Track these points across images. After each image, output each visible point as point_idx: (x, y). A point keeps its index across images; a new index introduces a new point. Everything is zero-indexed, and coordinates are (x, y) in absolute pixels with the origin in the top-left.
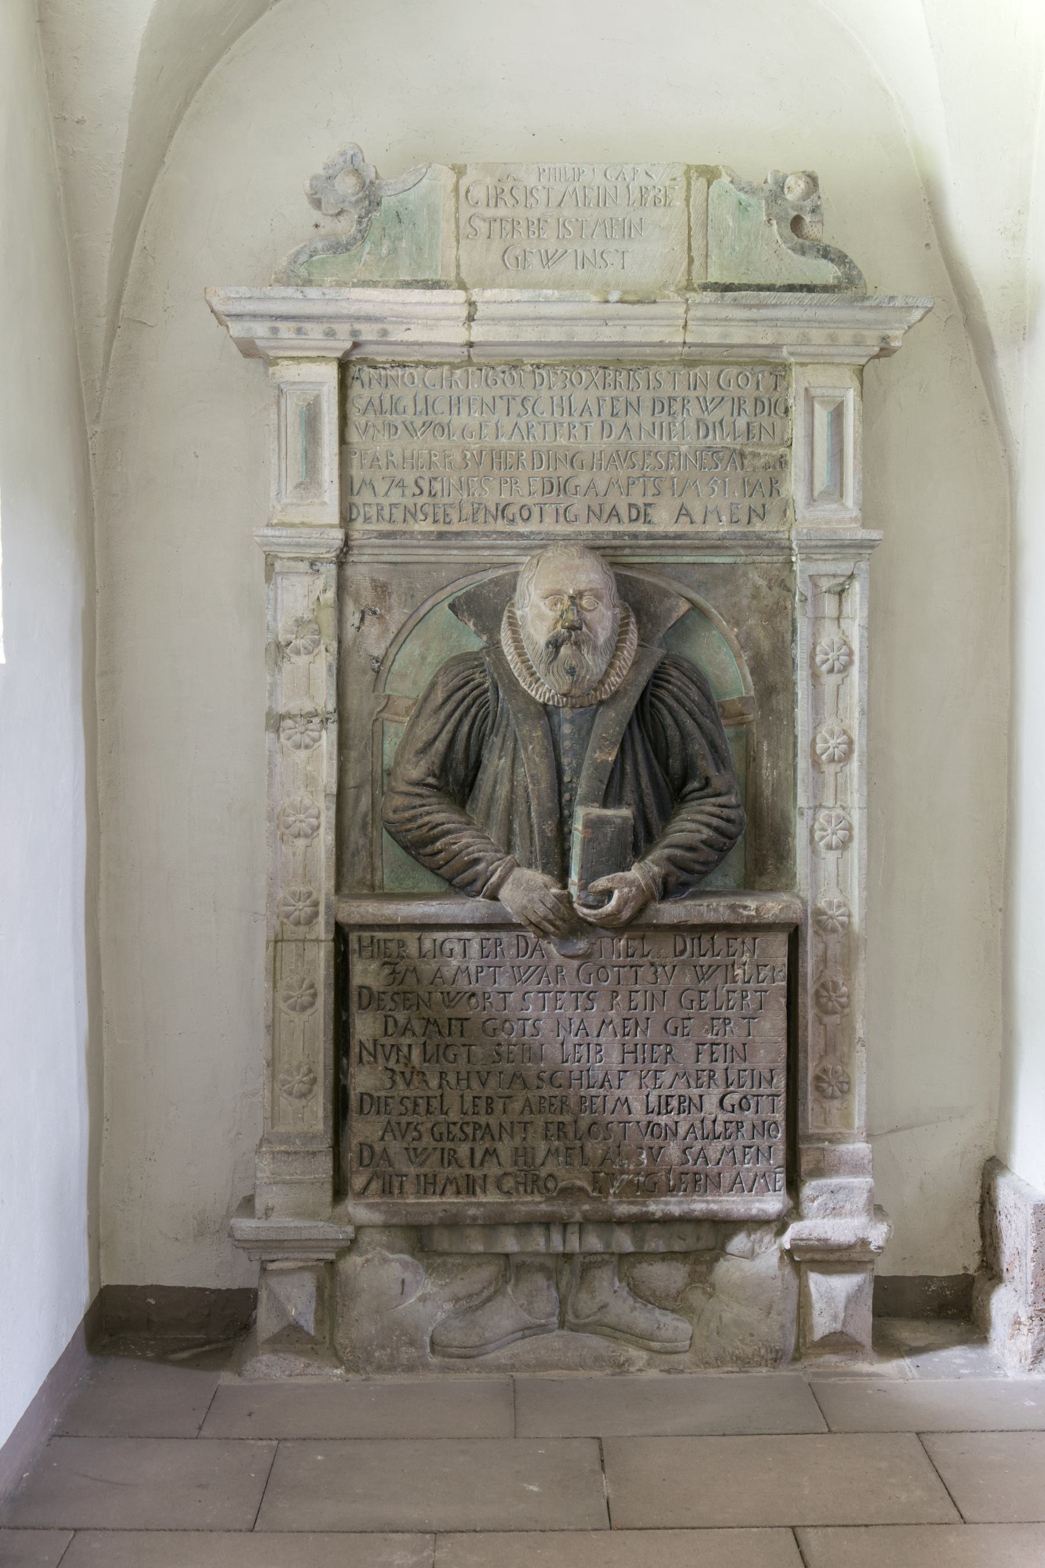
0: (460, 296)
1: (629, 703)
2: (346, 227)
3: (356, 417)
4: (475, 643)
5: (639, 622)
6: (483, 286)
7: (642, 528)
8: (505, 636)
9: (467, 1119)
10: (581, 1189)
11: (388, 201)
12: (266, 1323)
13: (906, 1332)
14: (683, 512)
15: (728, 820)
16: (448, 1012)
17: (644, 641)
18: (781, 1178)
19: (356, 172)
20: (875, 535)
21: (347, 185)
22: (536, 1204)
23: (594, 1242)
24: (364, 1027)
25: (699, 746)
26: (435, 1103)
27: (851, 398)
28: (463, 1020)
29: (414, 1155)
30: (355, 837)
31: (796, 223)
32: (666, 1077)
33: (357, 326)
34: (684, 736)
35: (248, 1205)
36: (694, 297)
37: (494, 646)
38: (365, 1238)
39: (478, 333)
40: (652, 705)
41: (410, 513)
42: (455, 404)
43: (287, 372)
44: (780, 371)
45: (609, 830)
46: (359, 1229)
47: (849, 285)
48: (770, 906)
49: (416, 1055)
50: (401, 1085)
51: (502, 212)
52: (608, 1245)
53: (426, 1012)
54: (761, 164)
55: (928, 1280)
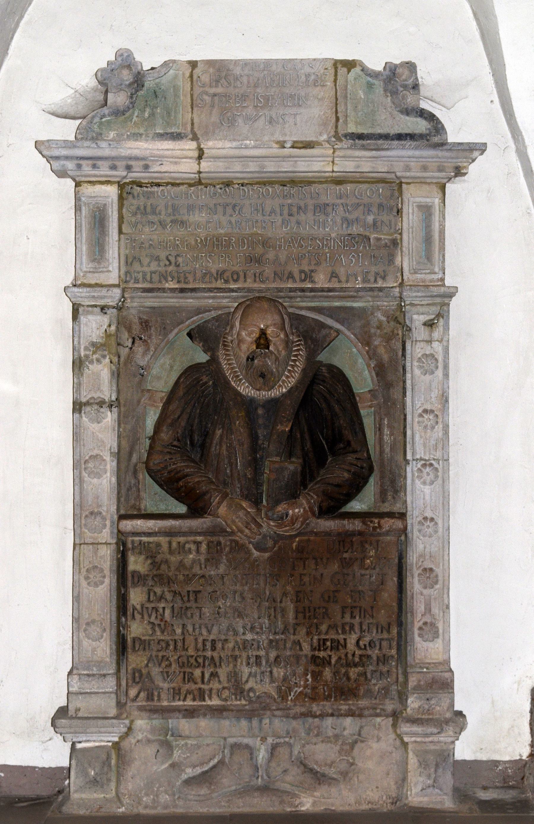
0: (193, 145)
4: (203, 357)
9: (200, 653)
11: (149, 83)
14: (334, 275)
21: (127, 76)
26: (180, 644)
29: (165, 675)
33: (131, 163)
37: (214, 360)
42: (191, 208)
43: (88, 190)
51: (219, 90)
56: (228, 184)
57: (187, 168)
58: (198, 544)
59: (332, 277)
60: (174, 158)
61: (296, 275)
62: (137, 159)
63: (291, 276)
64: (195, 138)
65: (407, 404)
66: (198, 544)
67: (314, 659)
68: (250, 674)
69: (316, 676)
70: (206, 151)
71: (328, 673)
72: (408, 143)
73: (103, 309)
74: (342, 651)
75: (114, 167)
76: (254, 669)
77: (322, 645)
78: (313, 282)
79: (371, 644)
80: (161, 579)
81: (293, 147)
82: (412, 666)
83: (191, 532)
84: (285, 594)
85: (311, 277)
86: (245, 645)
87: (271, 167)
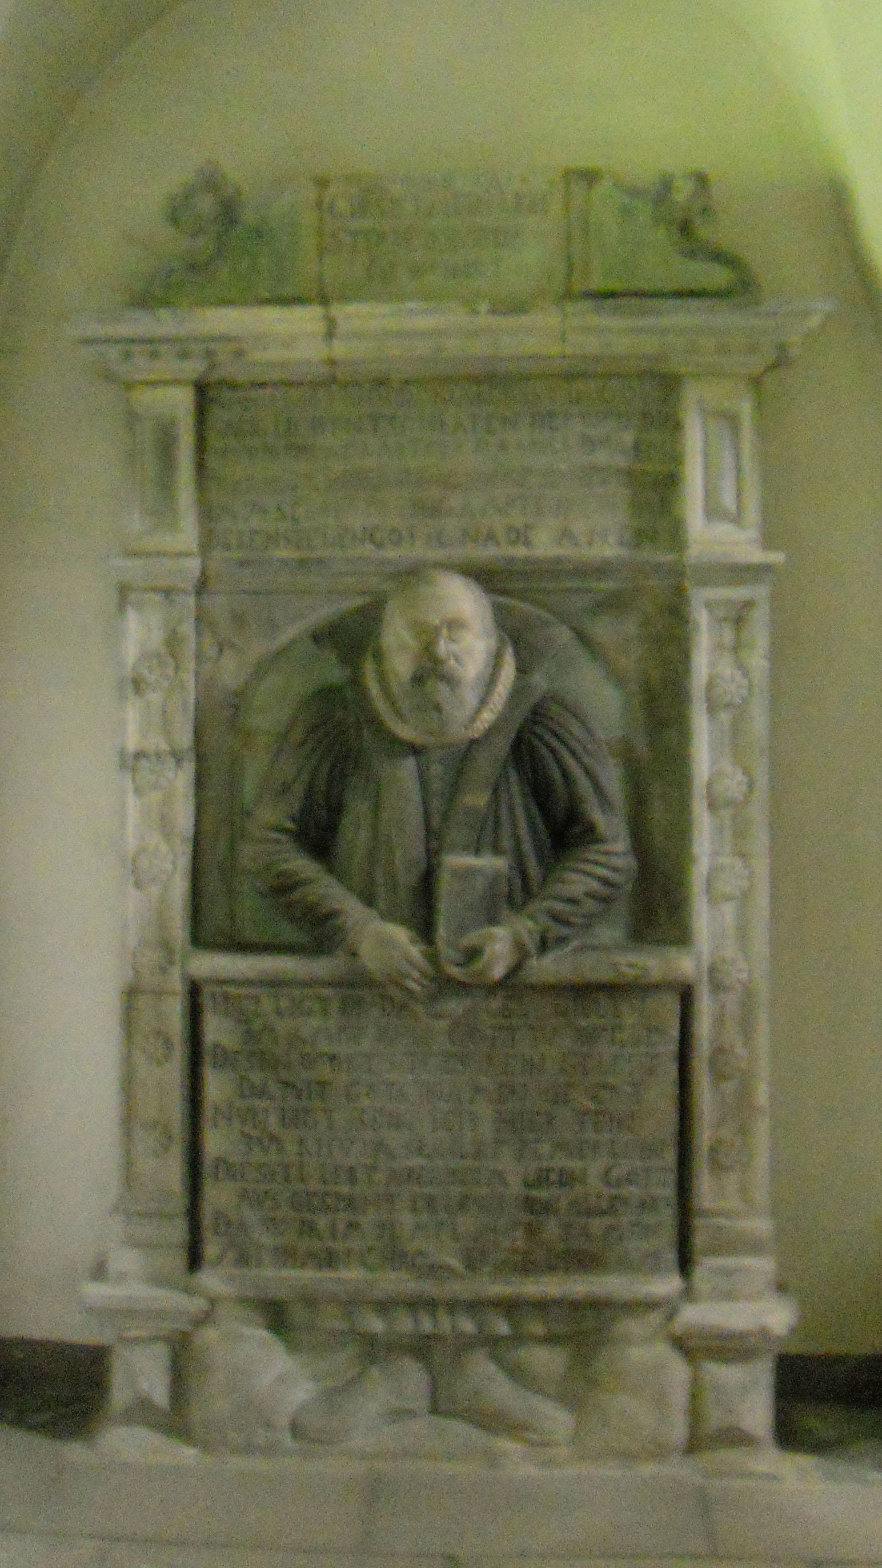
1: (502, 745)
2: (204, 244)
3: (214, 441)
5: (517, 653)
6: (344, 299)
7: (520, 552)
8: (369, 667)
9: (329, 1188)
10: (450, 1269)
11: (249, 216)
13: (814, 1421)
14: (566, 535)
15: (615, 869)
16: (305, 1075)
17: (522, 670)
18: (671, 1256)
20: (776, 558)
21: (206, 204)
22: (396, 1282)
23: (467, 1326)
24: (216, 1086)
25: (584, 786)
26: (293, 1172)
27: (746, 409)
29: (271, 1223)
30: (212, 883)
31: (685, 228)
33: (212, 346)
34: (566, 774)
35: (99, 1272)
36: (570, 307)
37: (356, 681)
39: (340, 349)
40: (530, 743)
41: (272, 539)
42: (317, 425)
43: (146, 399)
44: (667, 385)
45: (480, 884)
46: (213, 1302)
47: (742, 288)
48: (651, 963)
49: (273, 1122)
51: (365, 224)
52: (480, 1326)
53: (284, 1074)
55: (841, 1359)
56: (381, 382)
58: (323, 1000)
60: (285, 335)
61: (500, 534)
62: (225, 338)
63: (491, 537)
65: (592, 1279)
66: (323, 1000)
67: (529, 1204)
68: (418, 1227)
69: (532, 1231)
70: (340, 322)
71: (551, 1229)
72: (694, 303)
73: (168, 593)
74: (579, 1189)
77: (542, 1179)
78: (527, 543)
80: (265, 1061)
81: (493, 311)
86: (411, 1175)
87: (453, 346)
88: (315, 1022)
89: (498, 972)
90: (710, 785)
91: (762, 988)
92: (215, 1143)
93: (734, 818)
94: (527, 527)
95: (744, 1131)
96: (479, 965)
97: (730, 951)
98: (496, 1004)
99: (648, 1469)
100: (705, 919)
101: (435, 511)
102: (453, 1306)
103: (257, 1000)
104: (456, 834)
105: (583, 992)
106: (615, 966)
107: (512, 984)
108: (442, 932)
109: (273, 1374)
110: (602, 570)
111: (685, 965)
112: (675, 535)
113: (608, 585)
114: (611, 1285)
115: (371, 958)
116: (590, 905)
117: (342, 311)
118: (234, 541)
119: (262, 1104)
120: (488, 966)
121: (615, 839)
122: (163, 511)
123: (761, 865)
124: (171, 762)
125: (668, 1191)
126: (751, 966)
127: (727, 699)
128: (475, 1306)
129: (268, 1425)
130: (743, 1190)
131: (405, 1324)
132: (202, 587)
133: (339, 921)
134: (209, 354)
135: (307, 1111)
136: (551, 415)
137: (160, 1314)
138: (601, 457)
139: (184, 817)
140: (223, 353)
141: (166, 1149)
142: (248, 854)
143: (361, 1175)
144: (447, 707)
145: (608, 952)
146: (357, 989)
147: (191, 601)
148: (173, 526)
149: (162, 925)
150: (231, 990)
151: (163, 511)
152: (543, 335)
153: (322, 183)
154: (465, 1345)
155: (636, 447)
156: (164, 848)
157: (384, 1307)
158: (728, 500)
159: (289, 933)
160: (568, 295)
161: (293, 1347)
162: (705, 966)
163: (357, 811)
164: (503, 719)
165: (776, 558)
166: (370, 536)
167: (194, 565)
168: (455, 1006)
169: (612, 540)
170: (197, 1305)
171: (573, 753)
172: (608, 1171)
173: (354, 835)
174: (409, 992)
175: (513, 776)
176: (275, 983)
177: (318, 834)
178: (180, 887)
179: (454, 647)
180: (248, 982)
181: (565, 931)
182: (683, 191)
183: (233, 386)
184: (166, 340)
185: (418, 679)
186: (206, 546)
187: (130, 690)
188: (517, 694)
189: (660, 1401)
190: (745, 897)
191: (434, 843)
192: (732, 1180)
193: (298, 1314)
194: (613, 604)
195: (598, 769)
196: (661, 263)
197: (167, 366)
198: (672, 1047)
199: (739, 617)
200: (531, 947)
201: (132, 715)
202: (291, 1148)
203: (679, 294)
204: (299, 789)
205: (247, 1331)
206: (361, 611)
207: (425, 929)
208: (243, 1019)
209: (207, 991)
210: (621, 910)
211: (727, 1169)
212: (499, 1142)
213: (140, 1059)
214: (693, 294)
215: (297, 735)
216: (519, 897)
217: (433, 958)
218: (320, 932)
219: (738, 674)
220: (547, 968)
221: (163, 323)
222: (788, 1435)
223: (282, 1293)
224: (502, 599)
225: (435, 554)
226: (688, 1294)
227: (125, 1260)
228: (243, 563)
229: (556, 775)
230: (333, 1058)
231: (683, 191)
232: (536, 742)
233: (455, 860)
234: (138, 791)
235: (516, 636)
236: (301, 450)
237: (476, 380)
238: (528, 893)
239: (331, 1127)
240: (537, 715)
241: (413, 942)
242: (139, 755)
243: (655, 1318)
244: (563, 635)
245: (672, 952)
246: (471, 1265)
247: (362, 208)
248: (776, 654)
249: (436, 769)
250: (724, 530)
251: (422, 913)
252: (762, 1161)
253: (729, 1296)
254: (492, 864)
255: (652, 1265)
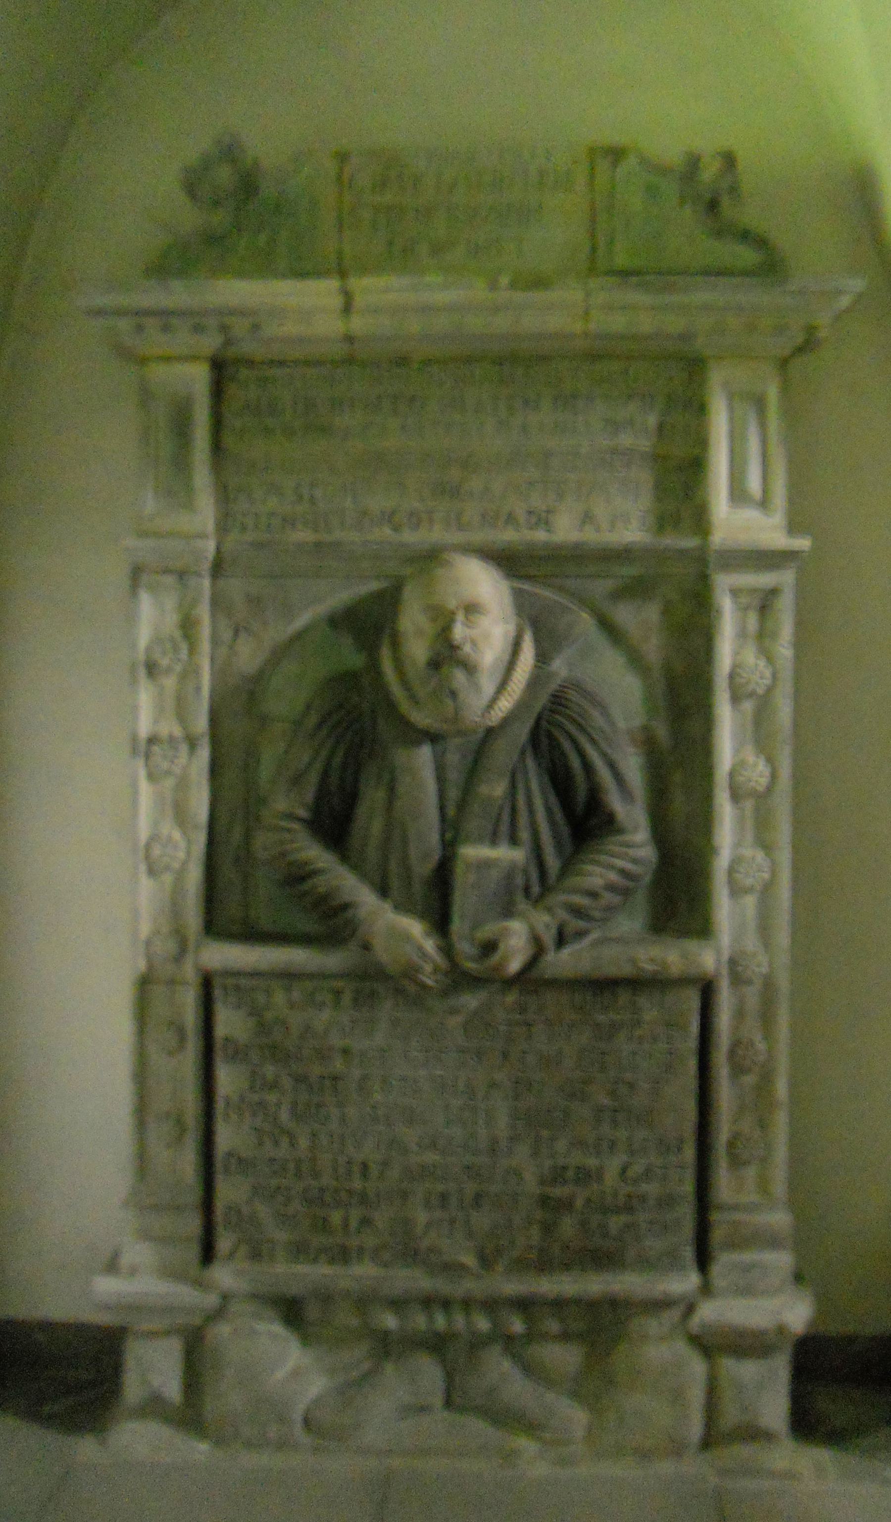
0: (334, 284)
1: (522, 732)
2: (220, 219)
4: (355, 660)
6: (364, 270)
7: (541, 536)
10: (463, 1267)
12: (133, 1390)
13: (830, 1405)
14: (587, 518)
15: (635, 861)
17: (542, 658)
18: (689, 1253)
19: (234, 161)
20: (803, 543)
21: (224, 175)
23: (483, 1324)
24: (227, 1079)
27: (773, 393)
28: (335, 1078)
30: (228, 873)
31: (713, 206)
32: (561, 1145)
35: (112, 1267)
36: (593, 283)
37: (374, 666)
38: (234, 1307)
39: (358, 324)
41: (289, 522)
43: (159, 372)
44: (695, 367)
45: (495, 874)
46: (226, 1297)
47: (771, 267)
48: (672, 956)
49: (284, 1116)
50: (268, 1144)
51: (388, 198)
52: (495, 1324)
54: (670, 149)
55: (851, 1339)
56: (402, 361)
57: (329, 326)
59: (584, 522)
60: (300, 308)
61: (522, 518)
63: (511, 519)
64: (343, 274)
66: (338, 993)
67: (544, 1201)
69: (548, 1229)
71: (568, 1226)
72: (723, 280)
75: (198, 329)
76: (438, 1214)
77: (558, 1175)
79: (648, 1175)
80: (276, 1053)
81: (513, 285)
82: (720, 1208)
83: (321, 976)
84: (493, 1085)
85: (547, 523)
86: (426, 1172)
88: (326, 1015)
89: (515, 966)
90: (732, 775)
91: (783, 982)
92: (226, 1138)
93: (757, 810)
94: (548, 512)
95: (763, 1124)
96: (495, 959)
97: (751, 943)
98: (511, 998)
99: (666, 1467)
100: (725, 910)
101: (454, 492)
102: (467, 1304)
103: (268, 992)
104: (473, 824)
105: (603, 986)
106: (633, 961)
107: (529, 979)
108: (457, 925)
109: (285, 1366)
110: (624, 555)
111: (708, 959)
112: (700, 521)
113: (630, 571)
114: (628, 1283)
115: (384, 953)
116: (609, 898)
117: (360, 284)
118: (250, 522)
119: (272, 1098)
120: (505, 960)
121: (636, 829)
122: (178, 492)
123: (785, 857)
124: (184, 748)
125: (689, 1187)
126: (773, 960)
127: (750, 687)
128: (491, 1305)
129: (282, 1419)
130: (763, 1186)
131: (419, 1321)
132: (218, 568)
133: (349, 913)
134: (224, 329)
135: (319, 1106)
136: (574, 396)
137: (169, 1310)
138: (626, 440)
139: (200, 804)
140: (240, 327)
141: (180, 1138)
142: (262, 842)
143: (374, 1170)
144: (461, 696)
145: (625, 943)
146: (373, 982)
147: (206, 583)
148: (189, 504)
149: (175, 910)
150: (243, 982)
151: (178, 492)
152: (564, 311)
153: (342, 157)
154: (477, 1344)
155: (661, 427)
156: (177, 835)
157: (398, 1304)
158: (754, 483)
159: (306, 924)
160: (592, 270)
161: (306, 1339)
162: (725, 957)
163: (372, 797)
164: (521, 707)
165: (803, 543)
166: (389, 517)
167: (210, 546)
168: (471, 1001)
169: (635, 524)
170: (211, 1300)
171: (593, 741)
172: (624, 1170)
173: (369, 821)
174: (424, 986)
175: (530, 763)
176: (288, 976)
177: (333, 823)
178: (195, 875)
179: (474, 633)
180: (255, 974)
181: (581, 924)
182: (710, 171)
183: (250, 363)
184: (182, 313)
185: (435, 664)
186: (222, 528)
187: (142, 672)
188: (535, 683)
189: (677, 1396)
190: (767, 891)
191: (452, 835)
192: (751, 1172)
193: (312, 1312)
194: (636, 590)
195: (616, 756)
196: (686, 237)
197: (183, 340)
198: (692, 1043)
199: (765, 602)
200: (549, 938)
201: (145, 697)
202: (303, 1143)
203: (707, 272)
204: (313, 778)
205: (262, 1327)
206: (378, 597)
207: (440, 921)
208: (255, 1012)
209: (217, 982)
210: (641, 899)
211: (747, 1163)
212: (513, 1139)
213: (153, 1049)
214: (721, 273)
215: (313, 720)
216: (536, 889)
217: (447, 950)
218: (332, 924)
219: (762, 663)
220: (563, 962)
221: (178, 294)
222: (805, 1424)
223: (294, 1290)
224: (526, 587)
225: (457, 537)
226: (706, 1289)
227: (138, 1253)
228: (259, 546)
229: (575, 763)
230: (345, 1052)
231: (710, 171)
232: (557, 733)
233: (472, 852)
234: (151, 777)
235: (540, 625)
236: (325, 430)
237: (499, 361)
238: (546, 888)
239: (343, 1120)
240: (558, 701)
241: (428, 934)
242: (152, 740)
243: (675, 1314)
244: (586, 620)
245: (691, 945)
246: (486, 1261)
247: (382, 184)
248: (800, 644)
249: (453, 758)
250: (750, 515)
251: (437, 901)
252: (781, 1153)
253: (747, 1291)
254: (504, 854)
255: (669, 1262)
